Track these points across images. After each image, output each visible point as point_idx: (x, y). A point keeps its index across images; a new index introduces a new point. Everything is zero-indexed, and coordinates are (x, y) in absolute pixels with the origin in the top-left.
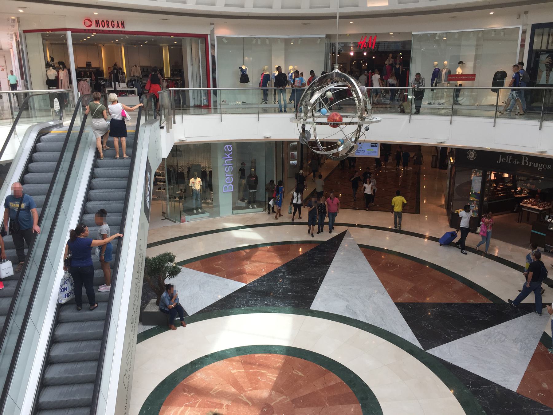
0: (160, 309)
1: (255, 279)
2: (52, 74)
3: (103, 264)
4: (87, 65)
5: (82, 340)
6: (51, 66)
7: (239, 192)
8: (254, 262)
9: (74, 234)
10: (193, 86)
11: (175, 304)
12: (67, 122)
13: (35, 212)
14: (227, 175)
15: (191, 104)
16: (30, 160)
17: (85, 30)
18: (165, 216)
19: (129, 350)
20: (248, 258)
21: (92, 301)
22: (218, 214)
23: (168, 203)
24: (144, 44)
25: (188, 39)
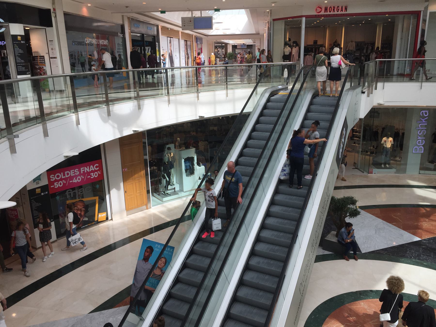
0: (338, 241)
1: (431, 236)
2: (288, 50)
3: (311, 155)
4: (314, 43)
5: (290, 207)
6: (288, 45)
7: (429, 154)
8: (433, 220)
9: (296, 133)
10: (400, 58)
11: (351, 239)
12: (290, 87)
13: (241, 188)
14: (420, 138)
15: (395, 72)
16: (261, 114)
17: (316, 15)
18: (355, 166)
19: (307, 266)
20: (427, 216)
21: (300, 183)
22: (404, 171)
23: (360, 155)
24: (362, 24)
25: (401, 16)
